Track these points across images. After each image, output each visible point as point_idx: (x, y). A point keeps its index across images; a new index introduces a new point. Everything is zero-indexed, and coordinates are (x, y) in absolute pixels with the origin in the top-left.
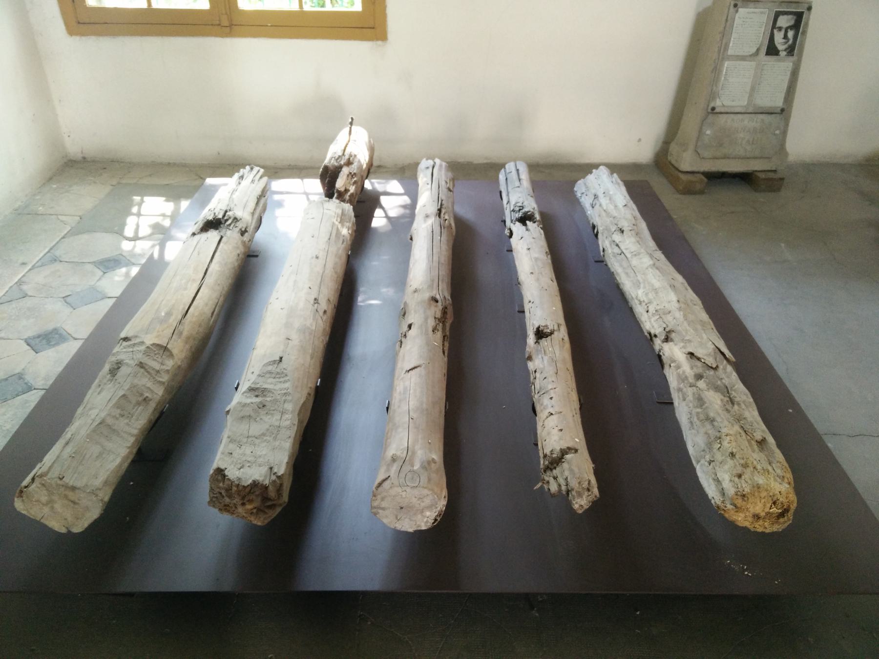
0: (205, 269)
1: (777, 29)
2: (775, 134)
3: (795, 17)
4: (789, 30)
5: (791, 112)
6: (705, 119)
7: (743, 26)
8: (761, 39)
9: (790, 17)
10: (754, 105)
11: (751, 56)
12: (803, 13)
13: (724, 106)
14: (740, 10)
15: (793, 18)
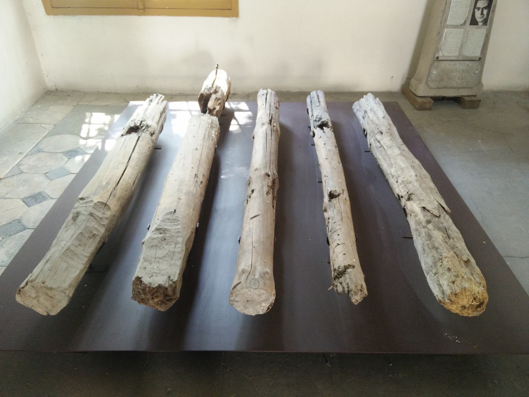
1: (477, 9)
2: (475, 73)
7: (457, 7)
8: (467, 14)
11: (461, 25)
15: (487, 2)
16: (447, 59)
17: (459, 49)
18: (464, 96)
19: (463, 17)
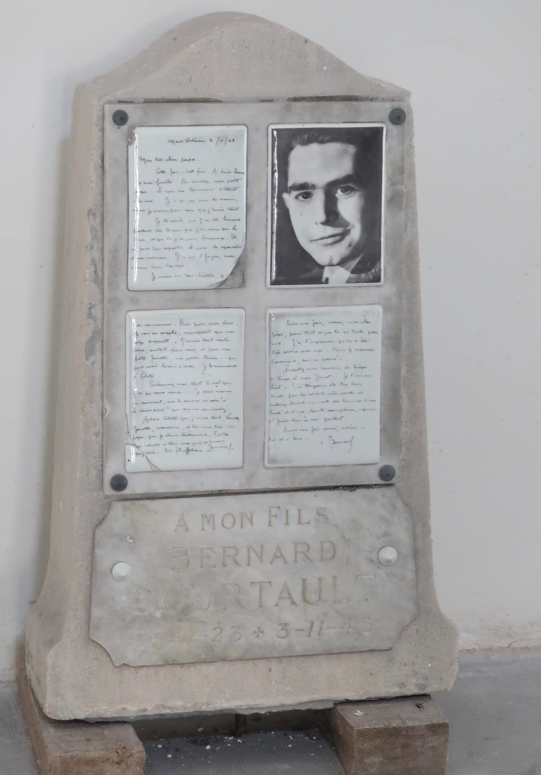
0: (266, 164)
1: (295, 193)
2: (381, 564)
3: (352, 149)
4: (339, 194)
5: (424, 407)
6: (100, 523)
7: (165, 187)
8: (241, 227)
9: (334, 147)
10: (272, 461)
11: (221, 286)
12: (378, 132)
13: (156, 471)
14: (138, 132)
15: (345, 152)
16: (182, 487)
17: (239, 425)
18: (348, 702)
19: (218, 243)
